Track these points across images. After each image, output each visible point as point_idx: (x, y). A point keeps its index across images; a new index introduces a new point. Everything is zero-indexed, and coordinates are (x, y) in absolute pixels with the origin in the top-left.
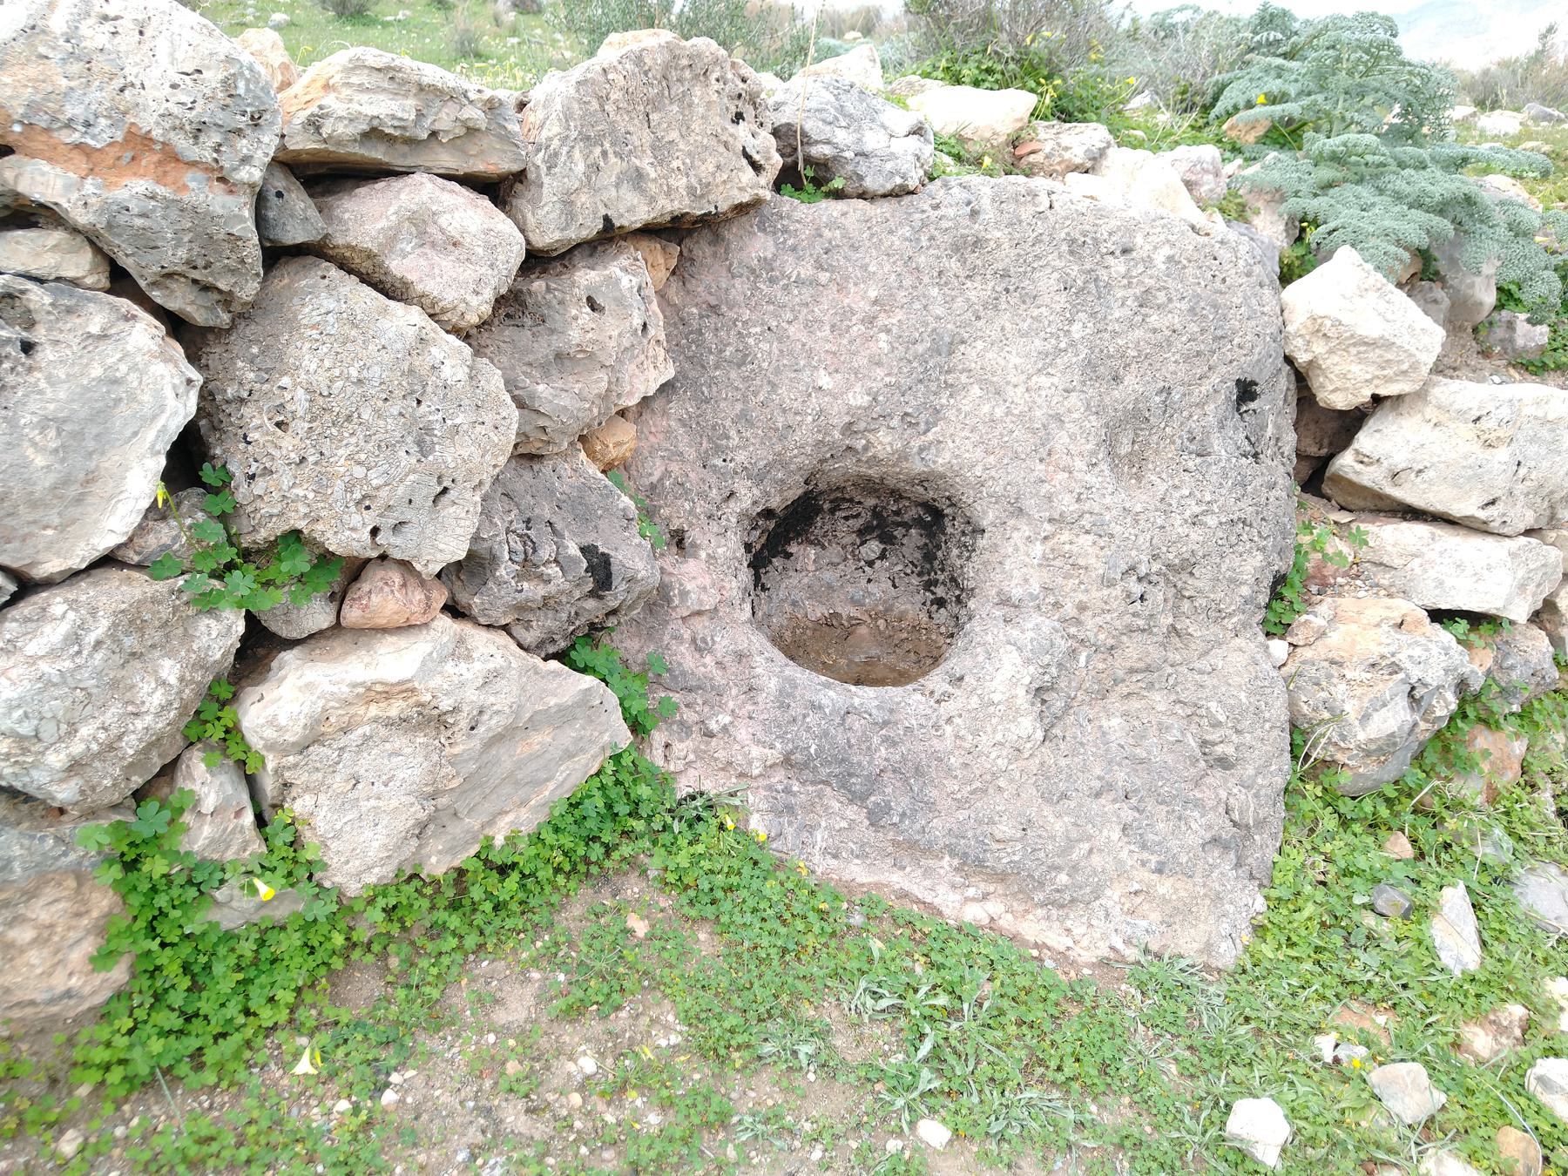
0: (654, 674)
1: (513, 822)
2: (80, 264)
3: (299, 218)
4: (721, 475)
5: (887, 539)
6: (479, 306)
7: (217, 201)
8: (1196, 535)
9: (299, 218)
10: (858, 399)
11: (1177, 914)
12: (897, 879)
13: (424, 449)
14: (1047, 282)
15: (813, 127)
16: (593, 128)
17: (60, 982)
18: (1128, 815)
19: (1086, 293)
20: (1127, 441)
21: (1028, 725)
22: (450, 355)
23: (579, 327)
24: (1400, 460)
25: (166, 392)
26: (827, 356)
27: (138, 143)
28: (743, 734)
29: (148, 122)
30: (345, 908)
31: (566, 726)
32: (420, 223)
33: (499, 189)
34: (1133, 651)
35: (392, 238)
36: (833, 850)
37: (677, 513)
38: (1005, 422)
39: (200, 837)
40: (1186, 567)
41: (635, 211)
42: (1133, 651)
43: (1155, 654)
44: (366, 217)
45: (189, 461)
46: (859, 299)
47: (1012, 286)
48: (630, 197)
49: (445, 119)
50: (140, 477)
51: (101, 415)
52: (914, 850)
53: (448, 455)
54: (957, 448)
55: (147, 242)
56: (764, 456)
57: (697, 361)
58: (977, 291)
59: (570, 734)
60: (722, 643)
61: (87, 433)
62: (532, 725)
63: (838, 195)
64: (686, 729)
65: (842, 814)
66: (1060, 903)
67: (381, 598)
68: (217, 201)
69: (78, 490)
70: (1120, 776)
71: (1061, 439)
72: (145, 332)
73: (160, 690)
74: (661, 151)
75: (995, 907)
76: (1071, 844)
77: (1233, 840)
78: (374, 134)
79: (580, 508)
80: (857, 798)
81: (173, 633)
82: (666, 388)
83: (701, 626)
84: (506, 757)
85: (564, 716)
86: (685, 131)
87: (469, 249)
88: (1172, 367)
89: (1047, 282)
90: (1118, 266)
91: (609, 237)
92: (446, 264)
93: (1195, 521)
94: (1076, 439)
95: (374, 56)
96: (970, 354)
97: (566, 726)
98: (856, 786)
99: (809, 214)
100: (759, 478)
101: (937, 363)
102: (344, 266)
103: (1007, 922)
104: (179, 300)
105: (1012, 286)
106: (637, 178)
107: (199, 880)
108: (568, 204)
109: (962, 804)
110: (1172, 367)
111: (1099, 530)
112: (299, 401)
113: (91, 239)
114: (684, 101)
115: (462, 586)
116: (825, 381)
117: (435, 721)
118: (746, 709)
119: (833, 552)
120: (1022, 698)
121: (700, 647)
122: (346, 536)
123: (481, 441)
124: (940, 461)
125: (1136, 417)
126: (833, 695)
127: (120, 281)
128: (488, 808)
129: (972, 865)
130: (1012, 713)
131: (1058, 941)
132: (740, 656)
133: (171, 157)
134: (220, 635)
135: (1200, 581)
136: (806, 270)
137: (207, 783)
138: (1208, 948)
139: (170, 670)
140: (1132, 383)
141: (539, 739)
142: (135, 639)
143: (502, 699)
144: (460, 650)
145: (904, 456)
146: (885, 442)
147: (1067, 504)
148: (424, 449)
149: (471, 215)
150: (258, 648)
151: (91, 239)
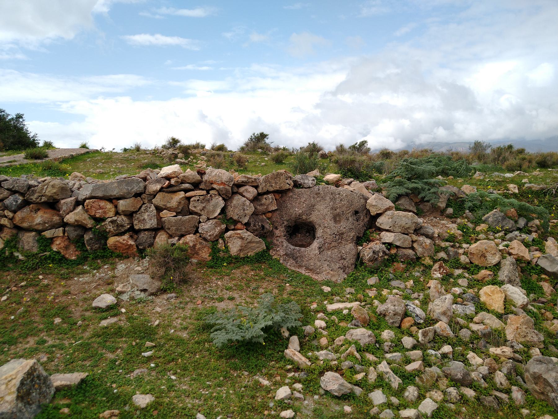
0: (272, 243)
1: (251, 254)
2: (216, 193)
3: (235, 189)
4: (282, 220)
5: (309, 233)
6: (251, 198)
7: (228, 187)
8: (344, 230)
9: (235, 189)
10: (300, 212)
11: (333, 276)
12: (298, 270)
13: (244, 211)
14: (328, 198)
15: (298, 180)
16: (266, 181)
17: (206, 257)
18: (328, 263)
19: (333, 199)
20: (336, 218)
21: (317, 252)
22: (248, 202)
23: (264, 201)
24: (381, 222)
25: (222, 203)
26: (296, 207)
27: (222, 183)
28: (281, 251)
29: (223, 181)
30: (231, 256)
31: (260, 245)
32: (246, 190)
33: (256, 187)
34: (333, 244)
35: (244, 191)
36: (290, 265)
37: (276, 224)
38: (322, 215)
39: (219, 246)
40: (343, 234)
41: (271, 189)
42: (333, 244)
43: (336, 245)
44: (242, 190)
45: (223, 211)
46: (303, 200)
47: (323, 198)
48: (271, 188)
49: (250, 180)
50: (219, 211)
51: (216, 205)
52: (300, 266)
53: (246, 212)
54: (314, 218)
55: (222, 191)
56: (288, 218)
57: (281, 207)
58: (318, 199)
59: (258, 245)
60: (280, 240)
61: (215, 206)
62: (253, 242)
63: (302, 188)
64: (274, 250)
65: (291, 261)
66: (318, 273)
67: (239, 226)
68: (228, 187)
69: (214, 211)
70: (328, 259)
71: (327, 217)
72: (221, 198)
73: (218, 230)
74: (276, 183)
75: (309, 274)
76: (320, 266)
77: (344, 268)
78: (243, 182)
79: (262, 221)
80: (294, 260)
81: (220, 225)
82: (276, 210)
83: (278, 238)
84: (251, 245)
85: (257, 242)
86: (279, 181)
87: (251, 192)
88: (344, 209)
89: (328, 198)
90: (338, 196)
91: (268, 192)
92: (249, 194)
93: (344, 228)
94: (329, 217)
95: (243, 175)
96: (316, 207)
97: (260, 245)
98: (295, 259)
99: (297, 190)
100: (288, 221)
101: (312, 207)
102: (239, 194)
103: (311, 276)
104: (224, 196)
105: (323, 198)
106: (272, 186)
107: (219, 251)
108: (262, 188)
109: (307, 261)
110: (344, 209)
111: (330, 228)
112: (233, 205)
113: (217, 191)
114: (280, 178)
115: (247, 225)
116: (297, 209)
117: (242, 238)
118: (283, 247)
119: (303, 235)
120: (317, 249)
121: (277, 240)
122: (235, 218)
123: (250, 209)
124: (311, 220)
125: (338, 215)
126: (292, 247)
127: (219, 195)
128: (248, 251)
129: (307, 268)
130: (315, 250)
131: (316, 278)
132: (282, 242)
133: (225, 184)
134: (223, 226)
135: (345, 236)
136: (296, 197)
137: (221, 241)
138: (337, 280)
139: (219, 228)
140: (338, 210)
141: (254, 244)
142: (216, 225)
143: (250, 238)
144: (246, 233)
145: (307, 219)
146: (304, 217)
147: (326, 225)
148: (244, 211)
149: (251, 189)
150: (227, 230)
151: (217, 191)
